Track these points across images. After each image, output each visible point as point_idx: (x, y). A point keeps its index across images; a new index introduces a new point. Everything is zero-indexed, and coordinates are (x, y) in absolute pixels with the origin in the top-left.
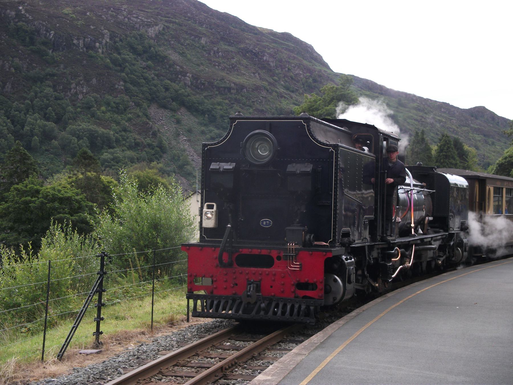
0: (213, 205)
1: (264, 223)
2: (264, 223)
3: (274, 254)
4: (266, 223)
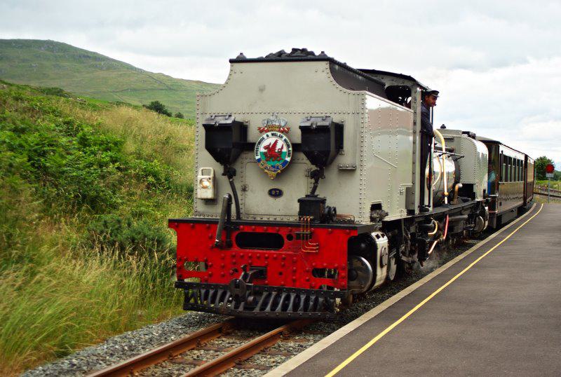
4: (276, 193)
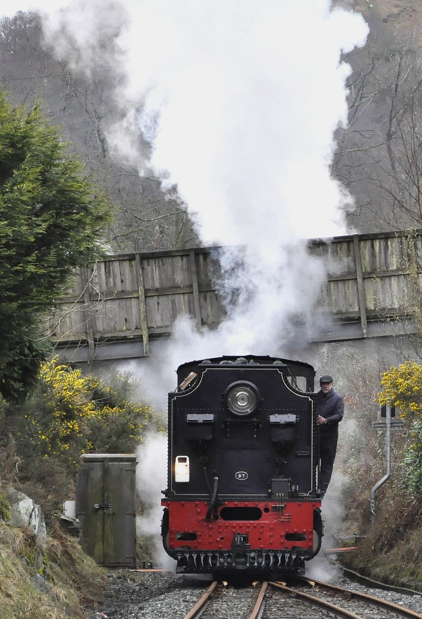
0: (186, 459)
1: (240, 476)
2: (240, 476)
3: (261, 506)
4: (242, 476)
